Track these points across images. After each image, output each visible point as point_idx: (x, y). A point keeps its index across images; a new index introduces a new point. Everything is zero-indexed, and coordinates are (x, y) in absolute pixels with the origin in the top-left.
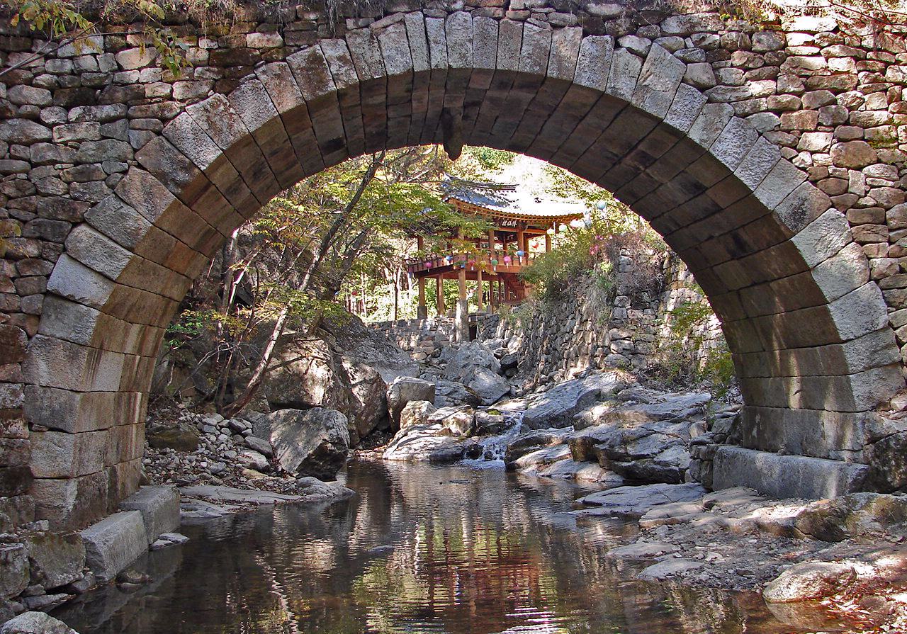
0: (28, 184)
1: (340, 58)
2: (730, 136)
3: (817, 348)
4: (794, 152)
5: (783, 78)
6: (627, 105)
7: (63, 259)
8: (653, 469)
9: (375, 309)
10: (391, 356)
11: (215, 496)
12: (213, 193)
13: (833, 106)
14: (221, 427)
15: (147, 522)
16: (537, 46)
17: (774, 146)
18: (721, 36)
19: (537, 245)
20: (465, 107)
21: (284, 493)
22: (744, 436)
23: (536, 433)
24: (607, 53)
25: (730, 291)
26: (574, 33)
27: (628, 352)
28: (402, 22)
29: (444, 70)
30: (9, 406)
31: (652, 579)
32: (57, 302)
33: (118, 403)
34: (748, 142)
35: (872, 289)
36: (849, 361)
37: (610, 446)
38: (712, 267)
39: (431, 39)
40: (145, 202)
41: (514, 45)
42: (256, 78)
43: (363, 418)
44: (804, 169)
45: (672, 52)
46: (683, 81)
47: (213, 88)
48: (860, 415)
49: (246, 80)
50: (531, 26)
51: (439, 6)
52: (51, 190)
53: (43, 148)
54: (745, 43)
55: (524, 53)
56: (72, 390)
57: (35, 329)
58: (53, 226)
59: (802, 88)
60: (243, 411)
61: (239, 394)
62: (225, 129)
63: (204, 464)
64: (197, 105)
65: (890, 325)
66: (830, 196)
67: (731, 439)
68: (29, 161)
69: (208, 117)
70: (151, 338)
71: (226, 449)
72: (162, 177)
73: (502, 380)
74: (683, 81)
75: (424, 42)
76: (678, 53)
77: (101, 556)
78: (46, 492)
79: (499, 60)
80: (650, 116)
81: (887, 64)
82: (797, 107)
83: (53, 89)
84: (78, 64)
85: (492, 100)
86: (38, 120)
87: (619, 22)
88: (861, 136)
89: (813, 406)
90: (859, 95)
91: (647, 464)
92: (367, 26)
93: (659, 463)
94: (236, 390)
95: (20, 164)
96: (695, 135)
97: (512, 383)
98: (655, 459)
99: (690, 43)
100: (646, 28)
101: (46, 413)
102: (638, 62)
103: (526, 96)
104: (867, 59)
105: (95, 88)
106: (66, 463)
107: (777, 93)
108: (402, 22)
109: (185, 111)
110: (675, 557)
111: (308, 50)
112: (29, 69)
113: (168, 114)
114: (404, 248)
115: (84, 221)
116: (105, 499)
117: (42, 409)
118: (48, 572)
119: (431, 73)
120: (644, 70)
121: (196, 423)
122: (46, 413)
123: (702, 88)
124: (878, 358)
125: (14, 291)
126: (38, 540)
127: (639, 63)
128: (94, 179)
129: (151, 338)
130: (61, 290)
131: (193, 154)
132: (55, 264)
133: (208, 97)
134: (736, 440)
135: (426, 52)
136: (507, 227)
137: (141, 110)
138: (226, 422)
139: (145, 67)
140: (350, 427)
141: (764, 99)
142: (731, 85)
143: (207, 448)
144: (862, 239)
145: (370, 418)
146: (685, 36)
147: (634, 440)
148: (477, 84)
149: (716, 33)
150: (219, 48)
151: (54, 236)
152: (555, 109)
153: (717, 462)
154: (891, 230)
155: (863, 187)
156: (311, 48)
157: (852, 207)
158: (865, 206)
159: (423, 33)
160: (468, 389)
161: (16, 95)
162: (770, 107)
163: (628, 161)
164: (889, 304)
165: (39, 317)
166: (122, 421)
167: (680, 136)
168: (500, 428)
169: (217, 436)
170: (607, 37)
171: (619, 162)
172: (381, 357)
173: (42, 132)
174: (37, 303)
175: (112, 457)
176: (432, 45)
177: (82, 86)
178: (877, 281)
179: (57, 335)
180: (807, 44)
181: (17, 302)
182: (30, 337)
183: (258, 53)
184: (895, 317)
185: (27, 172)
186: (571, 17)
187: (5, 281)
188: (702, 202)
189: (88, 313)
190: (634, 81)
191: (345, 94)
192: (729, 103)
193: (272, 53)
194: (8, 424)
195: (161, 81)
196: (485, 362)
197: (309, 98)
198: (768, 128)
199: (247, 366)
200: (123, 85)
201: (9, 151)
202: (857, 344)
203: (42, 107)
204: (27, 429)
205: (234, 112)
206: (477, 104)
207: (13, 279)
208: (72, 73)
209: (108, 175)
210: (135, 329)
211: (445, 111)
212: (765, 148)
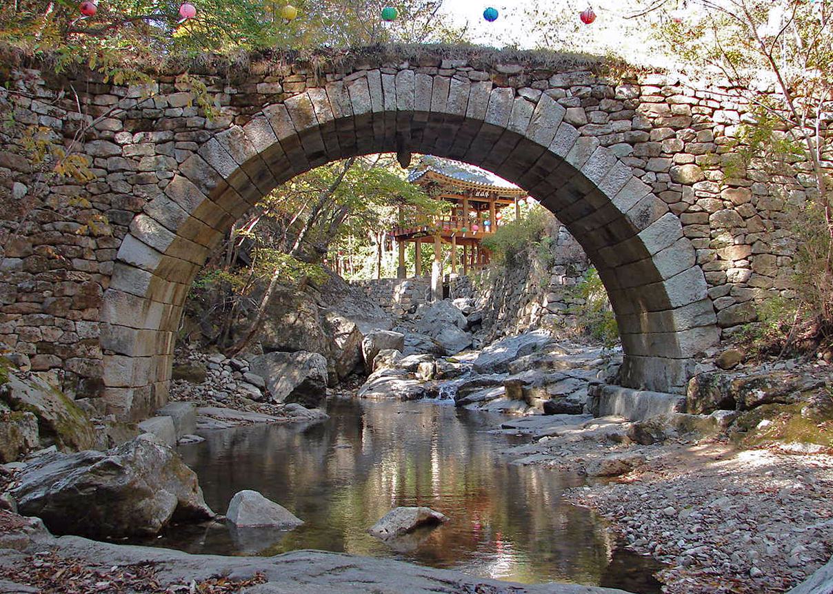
0: (106, 186)
1: (321, 102)
2: (596, 160)
6: (522, 137)
8: (566, 405)
9: (362, 267)
11: (222, 416)
12: (231, 191)
13: (673, 140)
14: (224, 365)
21: (275, 415)
23: (481, 377)
26: (486, 87)
28: (365, 77)
30: (91, 337)
33: (158, 339)
40: (185, 199)
42: (263, 115)
43: (342, 363)
46: (563, 120)
47: (233, 122)
50: (456, 81)
51: (392, 66)
52: (121, 189)
55: (451, 100)
58: (122, 214)
60: (241, 353)
61: (238, 339)
63: (211, 393)
65: (709, 296)
68: (106, 169)
70: (181, 292)
72: (197, 182)
74: (563, 120)
75: (380, 91)
76: (560, 101)
78: (112, 396)
81: (714, 109)
86: (113, 140)
88: (692, 161)
89: (660, 354)
90: (692, 131)
91: (562, 402)
92: (341, 80)
93: (570, 401)
94: (236, 335)
99: (569, 93)
105: (152, 119)
106: (126, 378)
108: (365, 77)
113: (202, 139)
114: (386, 213)
115: (142, 212)
116: (149, 407)
120: (536, 111)
121: (203, 361)
122: (114, 343)
124: (699, 320)
126: (113, 425)
129: (181, 292)
135: (381, 99)
136: (480, 197)
140: (330, 370)
141: (622, 134)
144: (690, 235)
145: (348, 363)
146: (566, 88)
148: (417, 118)
149: (589, 86)
150: (238, 93)
151: (122, 221)
154: (711, 229)
157: (684, 212)
158: (694, 212)
164: (708, 282)
165: (110, 277)
166: (160, 352)
167: (561, 160)
170: (510, 89)
171: (527, 171)
172: (359, 311)
174: (109, 267)
175: (153, 377)
176: (386, 94)
178: (701, 266)
180: (655, 94)
181: (96, 266)
182: (104, 290)
184: (713, 291)
185: (104, 177)
186: (484, 74)
190: (528, 120)
196: (452, 318)
197: (299, 130)
199: (245, 316)
200: (171, 118)
201: (93, 162)
203: (116, 132)
207: (94, 250)
210: (172, 285)
212: (621, 169)
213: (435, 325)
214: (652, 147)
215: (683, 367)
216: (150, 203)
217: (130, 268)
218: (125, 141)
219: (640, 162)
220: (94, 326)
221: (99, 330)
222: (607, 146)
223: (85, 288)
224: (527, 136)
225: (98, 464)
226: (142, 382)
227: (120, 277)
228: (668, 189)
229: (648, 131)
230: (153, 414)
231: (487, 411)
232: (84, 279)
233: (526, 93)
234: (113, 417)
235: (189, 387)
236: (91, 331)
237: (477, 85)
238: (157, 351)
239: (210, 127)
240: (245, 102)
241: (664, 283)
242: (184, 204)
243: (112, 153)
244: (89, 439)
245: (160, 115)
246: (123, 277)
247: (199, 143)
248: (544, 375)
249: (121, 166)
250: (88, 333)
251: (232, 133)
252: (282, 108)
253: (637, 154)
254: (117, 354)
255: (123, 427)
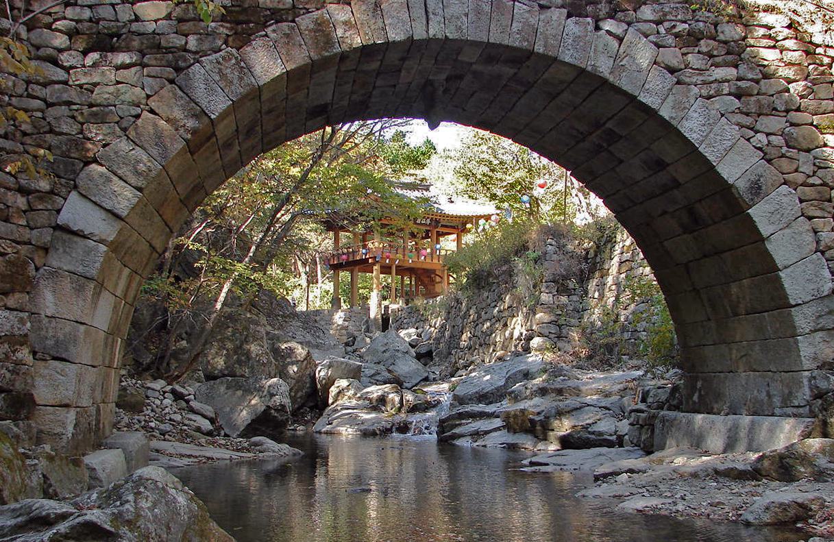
0: (43, 123)
1: (345, 23)
2: (696, 115)
3: (766, 314)
4: (752, 133)
5: (742, 67)
6: (605, 82)
7: (74, 195)
8: (588, 438)
10: (319, 337)
11: (172, 451)
13: (787, 94)
14: (165, 392)
15: (128, 460)
16: (526, 23)
17: (734, 126)
18: (689, 25)
19: (448, 244)
20: (447, 80)
21: (238, 450)
22: (684, 402)
24: (589, 33)
25: (678, 264)
27: (554, 335)
29: (442, 39)
30: (17, 333)
31: (631, 511)
32: (66, 236)
33: (106, 344)
34: (711, 121)
35: (819, 259)
36: (797, 324)
37: (545, 417)
38: (661, 243)
39: (430, 10)
40: (156, 145)
41: (506, 21)
42: (266, 35)
44: (760, 149)
45: (646, 37)
46: (655, 63)
47: (226, 42)
48: (807, 373)
49: (257, 37)
53: (59, 90)
54: (710, 32)
56: (77, 322)
57: (43, 261)
59: (761, 76)
62: (235, 82)
63: (152, 425)
64: (210, 57)
66: (783, 174)
67: (670, 405)
68: (45, 100)
69: (220, 69)
71: (171, 412)
73: (419, 366)
74: (655, 63)
75: (424, 13)
76: (652, 38)
77: (101, 481)
78: (46, 419)
79: (491, 34)
80: (625, 93)
82: (756, 92)
83: (72, 34)
84: (97, 13)
85: (475, 73)
86: (55, 62)
87: (599, 6)
93: (593, 433)
95: (37, 103)
96: (665, 113)
97: (429, 370)
98: (589, 430)
100: (623, 14)
101: (50, 343)
102: (615, 43)
103: (508, 71)
104: (815, 54)
105: (111, 36)
106: (67, 392)
107: (739, 79)
109: (198, 62)
110: (643, 496)
111: (316, 13)
112: (50, 14)
114: (321, 242)
115: (95, 161)
117: (47, 338)
118: (58, 490)
119: (428, 42)
120: (621, 50)
122: (50, 343)
123: (672, 71)
125: (25, 223)
126: (50, 458)
127: (617, 45)
128: (108, 121)
130: (71, 225)
131: (204, 104)
132: (65, 199)
133: (221, 50)
134: (674, 406)
135: (425, 22)
137: (156, 59)
138: (169, 388)
139: (161, 19)
141: (726, 84)
142: (697, 69)
143: (152, 411)
144: (810, 214)
145: (299, 394)
147: (569, 412)
148: (467, 56)
149: (685, 22)
150: (233, 6)
151: (66, 172)
152: (533, 86)
153: (658, 425)
155: (812, 168)
156: (319, 12)
157: (801, 185)
159: (423, 5)
160: (390, 371)
161: (36, 38)
162: (732, 91)
163: (594, 138)
165: (46, 250)
166: (107, 362)
167: (650, 113)
168: (426, 406)
169: (162, 401)
170: (589, 20)
172: (309, 337)
173: (60, 75)
174: (46, 236)
176: (431, 16)
177: (99, 33)
178: (823, 253)
179: (65, 268)
181: (27, 234)
183: (268, 13)
185: (42, 111)
187: (18, 213)
188: (662, 178)
189: (96, 249)
190: (613, 59)
191: (348, 57)
192: (695, 86)
193: (283, 14)
194: (15, 350)
195: (176, 33)
197: (316, 58)
198: (730, 110)
200: (139, 34)
201: (27, 90)
202: (805, 308)
203: (61, 51)
204: (31, 356)
205: (245, 66)
206: (460, 77)
207: (24, 212)
208: (90, 20)
209: (122, 118)
210: (126, 271)
211: (428, 83)
212: (726, 127)
213: (387, 355)
214: (763, 102)
215: (806, 382)
216: (107, 148)
217: (76, 239)
218: (72, 62)
219: (748, 121)
220: (22, 318)
221: (29, 324)
222: (709, 97)
223: (9, 262)
224: (611, 80)
225: (62, 527)
226: (85, 402)
227: (61, 250)
228: (783, 156)
229: (757, 82)
230: (98, 446)
231: (485, 446)
232: (9, 250)
233: (608, 25)
234: (47, 448)
235: (126, 417)
236: (17, 324)
237: (548, 13)
238: (103, 361)
239: (193, 49)
240: (242, 18)
241: (780, 273)
242: (154, 152)
243: (54, 78)
244: (18, 479)
245: (124, 30)
246: (65, 251)
247: (178, 70)
248: (556, 403)
249: (65, 97)
250: (12, 326)
251: (224, 58)
252: (293, 28)
253: (744, 110)
254: (55, 358)
255: (64, 461)
